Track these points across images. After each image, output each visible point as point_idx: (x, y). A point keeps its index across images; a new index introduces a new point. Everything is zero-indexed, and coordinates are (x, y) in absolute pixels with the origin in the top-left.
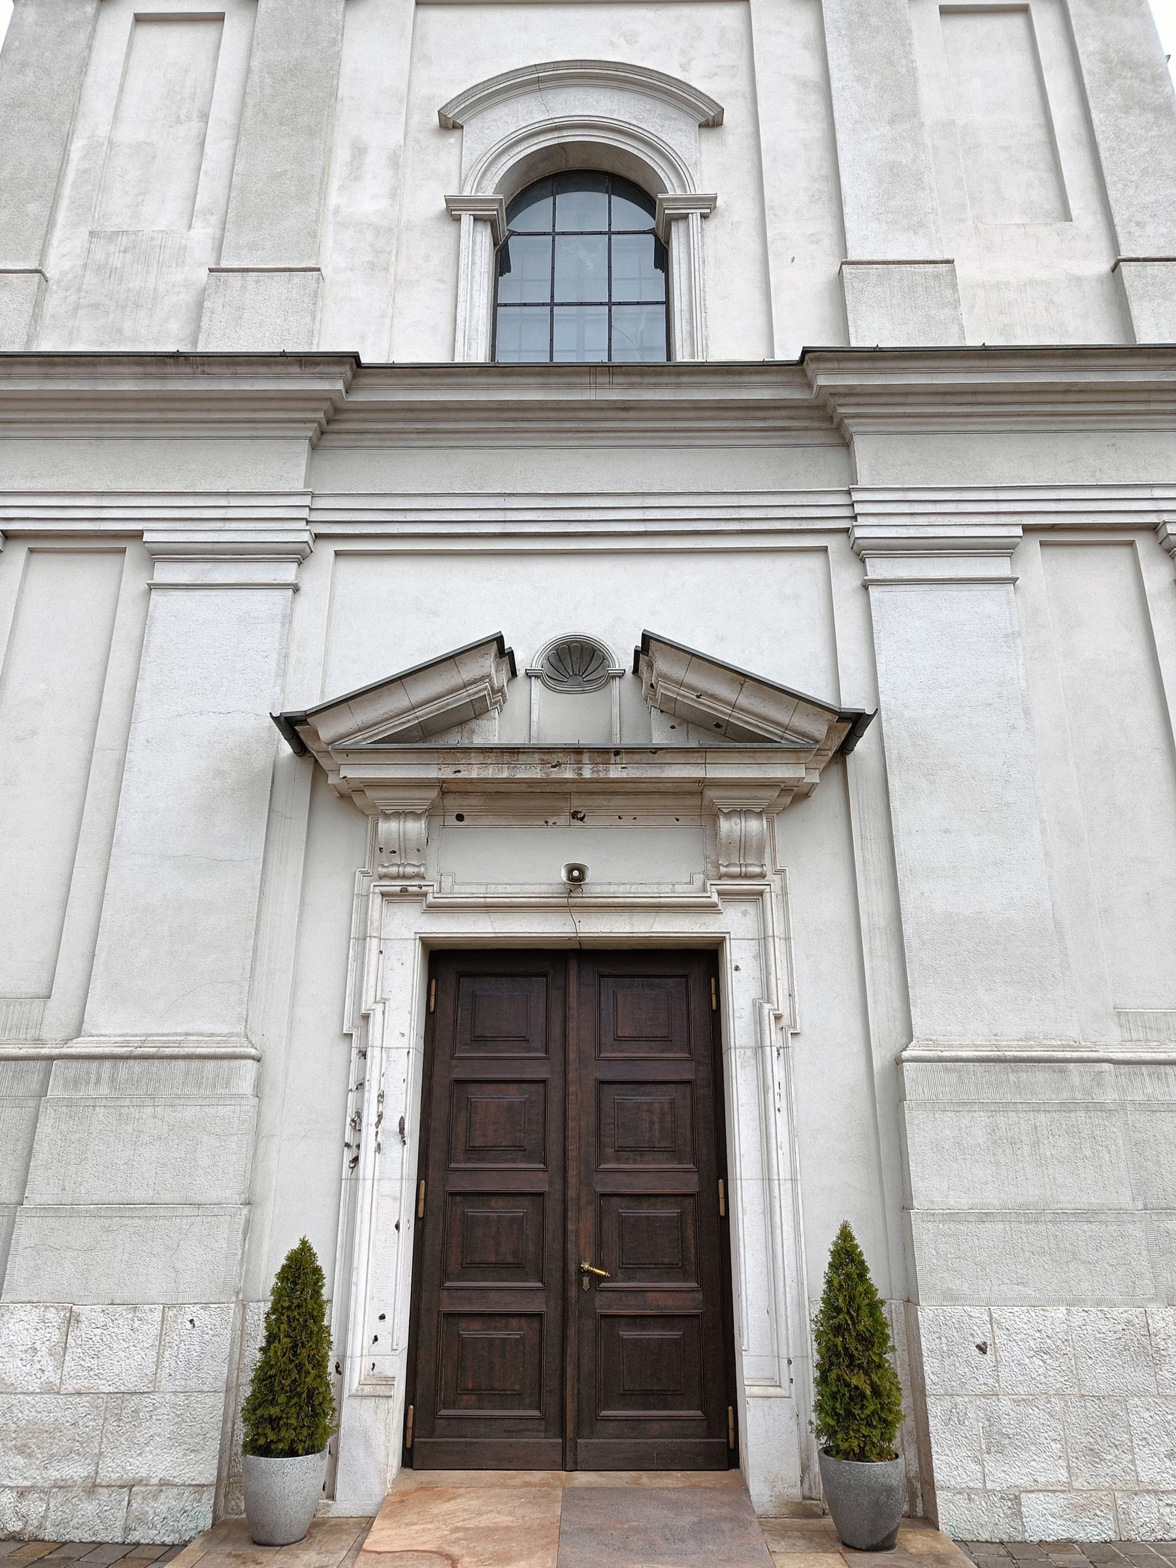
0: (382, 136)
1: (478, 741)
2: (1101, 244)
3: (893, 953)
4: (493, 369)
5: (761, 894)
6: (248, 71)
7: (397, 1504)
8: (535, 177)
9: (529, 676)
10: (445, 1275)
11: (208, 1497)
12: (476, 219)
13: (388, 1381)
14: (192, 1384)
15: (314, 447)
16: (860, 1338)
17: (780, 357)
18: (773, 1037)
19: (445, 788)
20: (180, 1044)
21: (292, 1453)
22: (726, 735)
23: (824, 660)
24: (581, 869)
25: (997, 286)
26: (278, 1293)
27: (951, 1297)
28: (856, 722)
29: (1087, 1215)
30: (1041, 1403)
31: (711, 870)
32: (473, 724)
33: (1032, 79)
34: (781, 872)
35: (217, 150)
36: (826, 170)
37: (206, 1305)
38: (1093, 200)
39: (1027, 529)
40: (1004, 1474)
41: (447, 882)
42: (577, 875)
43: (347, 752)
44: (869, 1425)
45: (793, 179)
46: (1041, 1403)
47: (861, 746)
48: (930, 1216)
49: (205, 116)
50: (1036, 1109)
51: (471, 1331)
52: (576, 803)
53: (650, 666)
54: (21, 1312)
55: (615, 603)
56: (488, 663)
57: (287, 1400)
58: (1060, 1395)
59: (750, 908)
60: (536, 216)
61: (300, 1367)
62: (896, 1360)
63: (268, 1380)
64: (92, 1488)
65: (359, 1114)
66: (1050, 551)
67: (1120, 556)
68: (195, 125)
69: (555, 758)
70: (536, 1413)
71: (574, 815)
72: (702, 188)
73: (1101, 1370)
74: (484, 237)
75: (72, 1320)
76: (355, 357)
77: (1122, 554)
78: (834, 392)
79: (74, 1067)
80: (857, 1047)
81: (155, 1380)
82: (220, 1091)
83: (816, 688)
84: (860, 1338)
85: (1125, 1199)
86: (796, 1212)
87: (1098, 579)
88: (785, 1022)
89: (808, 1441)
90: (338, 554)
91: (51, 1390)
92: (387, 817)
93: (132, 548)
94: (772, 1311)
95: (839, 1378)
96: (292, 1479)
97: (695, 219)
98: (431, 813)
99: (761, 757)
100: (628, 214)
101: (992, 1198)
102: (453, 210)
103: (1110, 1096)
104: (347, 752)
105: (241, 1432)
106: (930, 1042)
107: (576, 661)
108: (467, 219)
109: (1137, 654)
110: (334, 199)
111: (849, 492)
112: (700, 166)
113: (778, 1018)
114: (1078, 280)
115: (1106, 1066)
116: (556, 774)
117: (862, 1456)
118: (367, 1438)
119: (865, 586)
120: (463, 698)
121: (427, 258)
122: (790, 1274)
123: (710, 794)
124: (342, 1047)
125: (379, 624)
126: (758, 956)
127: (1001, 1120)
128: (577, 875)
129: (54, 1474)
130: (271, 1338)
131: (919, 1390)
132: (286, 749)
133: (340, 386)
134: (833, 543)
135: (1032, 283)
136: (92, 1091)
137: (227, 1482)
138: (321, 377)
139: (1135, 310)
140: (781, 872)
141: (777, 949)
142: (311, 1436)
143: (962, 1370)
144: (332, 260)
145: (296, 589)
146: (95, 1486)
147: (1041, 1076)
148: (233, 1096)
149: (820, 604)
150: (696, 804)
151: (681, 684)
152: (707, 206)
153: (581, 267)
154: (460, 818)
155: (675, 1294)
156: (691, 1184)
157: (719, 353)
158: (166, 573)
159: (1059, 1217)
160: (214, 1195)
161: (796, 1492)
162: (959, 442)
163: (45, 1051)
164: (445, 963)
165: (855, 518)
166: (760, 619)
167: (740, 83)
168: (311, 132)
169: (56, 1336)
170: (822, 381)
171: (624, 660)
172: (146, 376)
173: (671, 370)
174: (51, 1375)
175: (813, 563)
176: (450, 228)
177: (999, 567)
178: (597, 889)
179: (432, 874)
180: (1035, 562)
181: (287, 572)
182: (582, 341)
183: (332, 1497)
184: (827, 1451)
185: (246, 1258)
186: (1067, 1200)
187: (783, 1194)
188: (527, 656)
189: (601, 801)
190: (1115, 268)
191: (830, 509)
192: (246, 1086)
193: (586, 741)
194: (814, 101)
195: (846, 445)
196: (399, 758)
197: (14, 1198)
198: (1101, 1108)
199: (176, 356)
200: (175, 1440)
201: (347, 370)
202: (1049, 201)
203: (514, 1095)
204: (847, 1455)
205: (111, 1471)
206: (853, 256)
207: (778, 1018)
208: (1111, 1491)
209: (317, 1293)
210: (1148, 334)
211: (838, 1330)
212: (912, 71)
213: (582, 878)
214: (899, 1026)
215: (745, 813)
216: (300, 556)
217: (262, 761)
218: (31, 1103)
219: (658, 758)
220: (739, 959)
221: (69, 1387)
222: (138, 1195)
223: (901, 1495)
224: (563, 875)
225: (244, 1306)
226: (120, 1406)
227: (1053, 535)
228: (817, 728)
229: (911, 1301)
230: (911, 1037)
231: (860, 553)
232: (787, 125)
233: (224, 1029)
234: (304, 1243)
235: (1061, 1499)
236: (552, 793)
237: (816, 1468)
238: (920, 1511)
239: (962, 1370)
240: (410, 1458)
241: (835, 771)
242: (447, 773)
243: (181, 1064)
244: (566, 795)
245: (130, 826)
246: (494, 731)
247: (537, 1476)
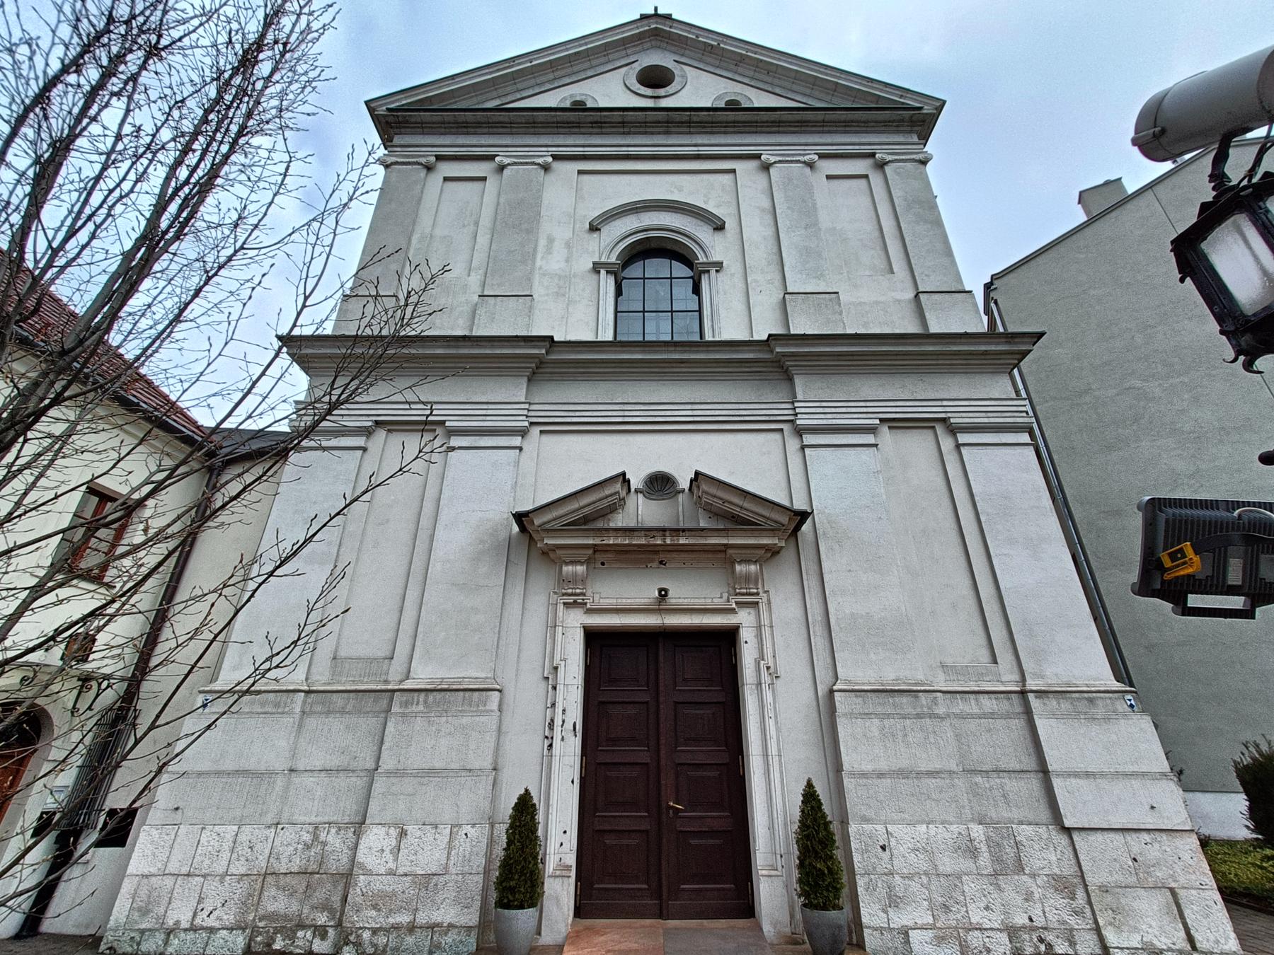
0: (563, 234)
1: (612, 525)
2: (909, 284)
3: (826, 634)
4: (615, 344)
5: (757, 603)
6: (498, 204)
7: (574, 937)
8: (634, 252)
9: (637, 491)
10: (596, 810)
11: (474, 934)
12: (608, 272)
13: (568, 868)
14: (466, 869)
15: (529, 380)
16: (821, 842)
17: (756, 338)
18: (766, 678)
19: (595, 548)
20: (460, 683)
21: (521, 907)
22: (739, 522)
23: (784, 484)
24: (666, 591)
25: (860, 304)
26: (512, 817)
27: (866, 820)
28: (803, 516)
29: (932, 774)
30: (916, 879)
31: (732, 591)
32: (610, 516)
33: (872, 208)
34: (767, 592)
35: (483, 240)
36: (775, 250)
37: (473, 825)
38: (904, 264)
39: (881, 420)
40: (900, 919)
41: (596, 599)
42: (663, 594)
43: (548, 531)
44: (828, 890)
45: (759, 254)
46: (916, 879)
47: (804, 528)
48: (852, 775)
49: (477, 224)
50: (904, 717)
51: (610, 841)
52: (662, 556)
53: (698, 487)
54: (376, 829)
55: (682, 457)
56: (618, 486)
57: (517, 877)
58: (926, 874)
59: (752, 611)
60: (635, 270)
61: (525, 859)
62: (838, 854)
63: (508, 866)
64: (412, 928)
65: (552, 720)
66: (894, 431)
67: (928, 435)
68: (472, 227)
69: (652, 534)
70: (645, 886)
71: (661, 562)
72: (716, 258)
73: (946, 859)
74: (611, 281)
75: (403, 834)
76: (552, 337)
77: (929, 433)
78: (784, 355)
79: (406, 696)
80: (809, 683)
81: (446, 866)
82: (481, 708)
83: (780, 498)
84: (821, 842)
85: (953, 766)
86: (781, 773)
87: (918, 445)
88: (772, 670)
89: (793, 901)
90: (541, 432)
91: (391, 873)
92: (567, 564)
93: (439, 430)
94: (771, 828)
95: (810, 864)
96: (523, 918)
97: (713, 272)
98: (588, 562)
99: (756, 533)
100: (680, 270)
101: (883, 766)
102: (596, 268)
103: (941, 710)
104: (548, 531)
105: (493, 896)
106: (848, 682)
107: (660, 484)
108: (603, 272)
109: (940, 481)
110: (539, 263)
111: (793, 403)
112: (716, 247)
113: (768, 668)
114: (899, 301)
115: (939, 694)
116: (652, 542)
117: (825, 908)
118: (558, 900)
119: (803, 448)
120: (605, 503)
121: (583, 290)
122: (780, 806)
123: (730, 551)
124: (543, 684)
125: (566, 466)
126: (756, 636)
127: (886, 722)
128: (663, 594)
129: (391, 920)
130: (510, 843)
131: (852, 872)
132: (516, 529)
133: (543, 351)
134: (785, 427)
135: (877, 303)
136: (414, 708)
137: (484, 925)
138: (534, 347)
139: (927, 314)
140: (767, 592)
141: (766, 632)
142: (531, 898)
143: (874, 860)
144: (538, 292)
145: (521, 449)
146: (414, 927)
147: (905, 699)
148: (487, 711)
149: (782, 456)
150: (723, 557)
151: (715, 496)
152: (719, 266)
153: (658, 294)
154: (603, 564)
155: (717, 818)
156: (725, 758)
157: (727, 335)
158: (456, 441)
159: (919, 775)
160: (477, 765)
161: (788, 930)
162: (845, 378)
163: (390, 687)
164: (593, 638)
165: (796, 415)
166: (750, 463)
167: (733, 210)
168: (528, 231)
169: (394, 843)
170: (778, 350)
171: (684, 484)
172: (448, 347)
173: (703, 345)
174: (391, 865)
175: (777, 436)
176: (595, 276)
177: (869, 439)
178: (673, 601)
179: (589, 593)
180: (886, 436)
181: (516, 441)
182: (658, 330)
183: (539, 934)
184: (805, 905)
185: (494, 799)
186: (923, 767)
187: (774, 762)
188: (636, 481)
189: (674, 555)
190: (917, 296)
191: (784, 411)
192: (495, 706)
193: (667, 525)
194: (768, 219)
195: (790, 380)
196: (575, 534)
197: (373, 766)
198: (937, 716)
199: (464, 337)
200: (456, 900)
201: (547, 344)
202: (882, 264)
203: (631, 710)
204: (817, 907)
205: (422, 918)
206: (790, 290)
207: (768, 668)
208: (956, 928)
209: (533, 818)
210: (934, 328)
211: (807, 837)
212: (814, 205)
213: (666, 595)
214: (831, 674)
215: (748, 561)
216: (523, 433)
217: (503, 535)
218: (383, 715)
219: (703, 534)
220: (747, 635)
221: (401, 871)
222: (438, 765)
223: (846, 930)
224: (657, 594)
225: (492, 825)
226: (426, 881)
227: (896, 424)
228: (784, 519)
229: (844, 822)
230: (837, 679)
231: (799, 432)
232: (756, 229)
233: (484, 675)
234: (526, 790)
235: (930, 934)
236: (646, 552)
237: (799, 916)
238: (855, 941)
239: (874, 860)
240: (579, 912)
241: (793, 539)
242: (597, 541)
243: (461, 694)
244: (656, 552)
245: (436, 568)
246: (619, 520)
247: (648, 922)
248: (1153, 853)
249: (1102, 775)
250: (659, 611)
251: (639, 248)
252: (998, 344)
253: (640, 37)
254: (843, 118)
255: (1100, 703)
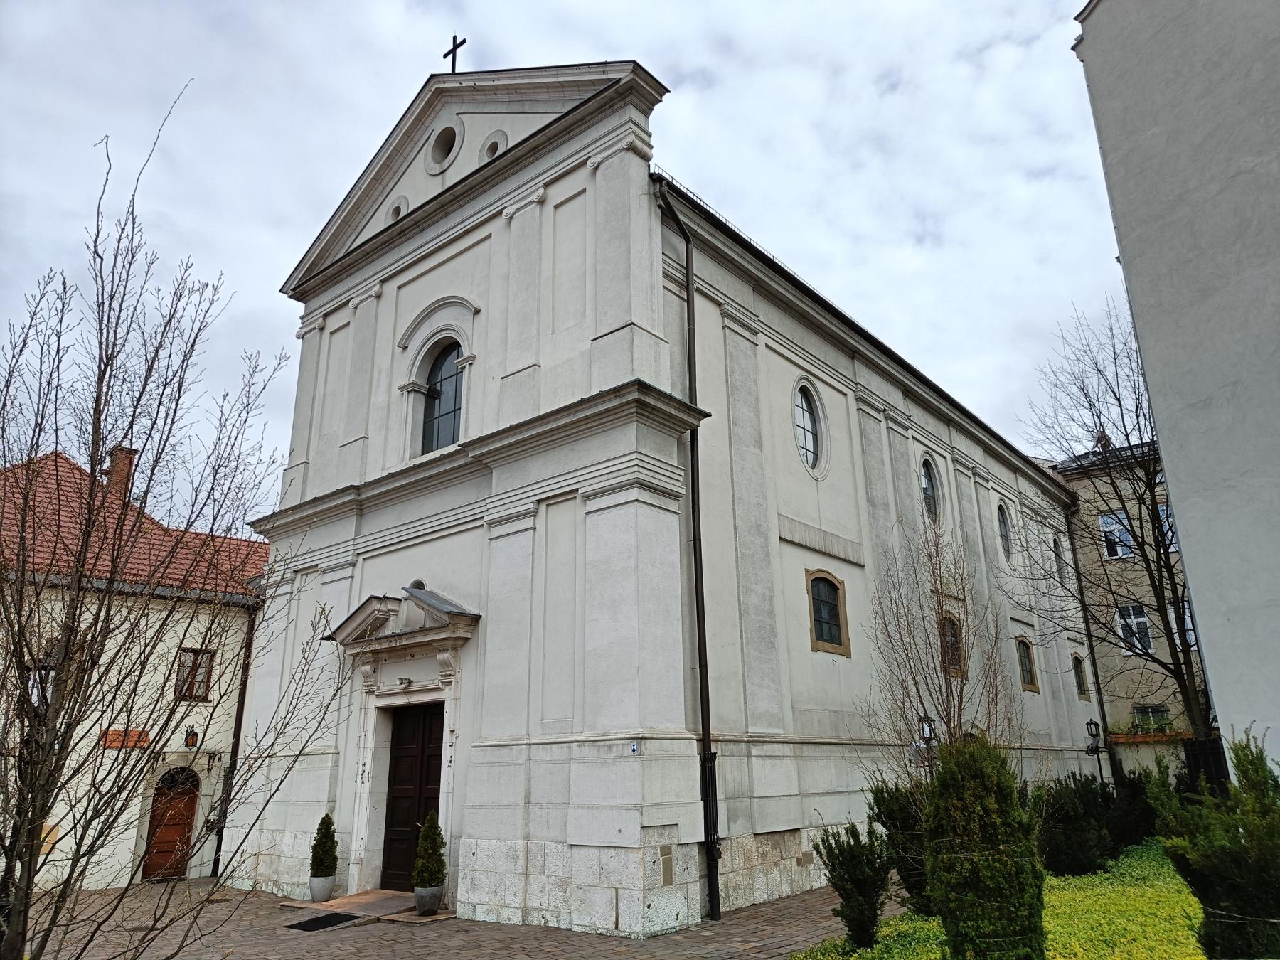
27: (470, 836)
248: (613, 864)
249: (598, 806)
250: (404, 692)
251: (437, 352)
252: (611, 400)
253: (429, 104)
254: (561, 127)
255: (614, 748)
